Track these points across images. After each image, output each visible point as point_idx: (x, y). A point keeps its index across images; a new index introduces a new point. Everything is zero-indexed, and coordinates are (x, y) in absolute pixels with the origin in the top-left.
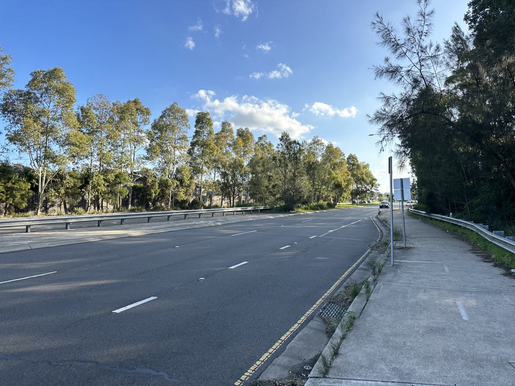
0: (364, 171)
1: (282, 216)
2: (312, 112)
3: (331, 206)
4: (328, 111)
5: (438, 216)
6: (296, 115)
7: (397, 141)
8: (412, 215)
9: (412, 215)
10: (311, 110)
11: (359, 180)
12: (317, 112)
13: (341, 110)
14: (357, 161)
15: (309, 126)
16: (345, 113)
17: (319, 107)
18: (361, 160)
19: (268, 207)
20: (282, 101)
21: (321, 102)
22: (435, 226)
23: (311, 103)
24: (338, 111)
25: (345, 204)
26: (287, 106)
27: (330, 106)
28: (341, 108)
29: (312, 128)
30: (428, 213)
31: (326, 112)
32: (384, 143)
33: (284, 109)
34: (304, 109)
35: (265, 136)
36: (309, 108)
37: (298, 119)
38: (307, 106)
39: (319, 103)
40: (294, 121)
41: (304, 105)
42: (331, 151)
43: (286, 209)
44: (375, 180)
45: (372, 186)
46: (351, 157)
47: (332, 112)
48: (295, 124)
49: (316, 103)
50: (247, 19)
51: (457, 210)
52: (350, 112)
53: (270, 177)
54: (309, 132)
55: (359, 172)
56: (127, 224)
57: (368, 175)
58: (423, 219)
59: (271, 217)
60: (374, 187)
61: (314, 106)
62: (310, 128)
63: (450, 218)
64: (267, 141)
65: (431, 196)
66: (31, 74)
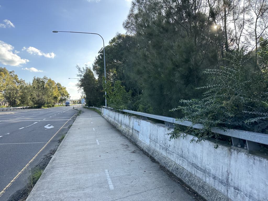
0: (64, 90)
1: (37, 110)
2: (28, 52)
3: (53, 106)
4: (38, 53)
5: (91, 107)
6: (18, 52)
7: (83, 90)
8: (84, 108)
9: (84, 108)
10: (28, 51)
11: (63, 95)
12: (32, 53)
13: (46, 54)
14: (61, 86)
15: (26, 59)
16: (48, 56)
17: (32, 49)
18: (63, 85)
19: (30, 106)
20: (9, 42)
21: (34, 47)
22: (90, 109)
23: (28, 47)
24: (44, 54)
25: (57, 105)
26: (11, 46)
27: (39, 51)
28: (46, 52)
29: (28, 61)
30: (89, 106)
31: (37, 54)
32: (79, 91)
33: (9, 47)
34: (23, 50)
35: (13, 71)
36: (26, 50)
37: (18, 55)
38: (24, 48)
39: (33, 48)
40: (16, 55)
41: (23, 47)
42: (51, 82)
43: (39, 107)
44: (69, 94)
45: (68, 97)
46: (58, 84)
47: (40, 54)
48: (16, 57)
49: (30, 47)
50: (48, 58)
51: (95, 105)
52: (51, 55)
53: (32, 94)
54: (26, 63)
55: (62, 91)
56: (4, 111)
57: (66, 92)
58: (88, 108)
59: (13, 113)
60: (68, 98)
61: (29, 48)
62: (26, 61)
63: (93, 107)
64: (15, 74)
65: (89, 102)
66: (24, 81)
